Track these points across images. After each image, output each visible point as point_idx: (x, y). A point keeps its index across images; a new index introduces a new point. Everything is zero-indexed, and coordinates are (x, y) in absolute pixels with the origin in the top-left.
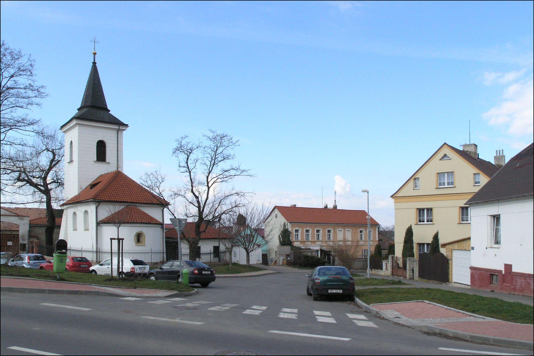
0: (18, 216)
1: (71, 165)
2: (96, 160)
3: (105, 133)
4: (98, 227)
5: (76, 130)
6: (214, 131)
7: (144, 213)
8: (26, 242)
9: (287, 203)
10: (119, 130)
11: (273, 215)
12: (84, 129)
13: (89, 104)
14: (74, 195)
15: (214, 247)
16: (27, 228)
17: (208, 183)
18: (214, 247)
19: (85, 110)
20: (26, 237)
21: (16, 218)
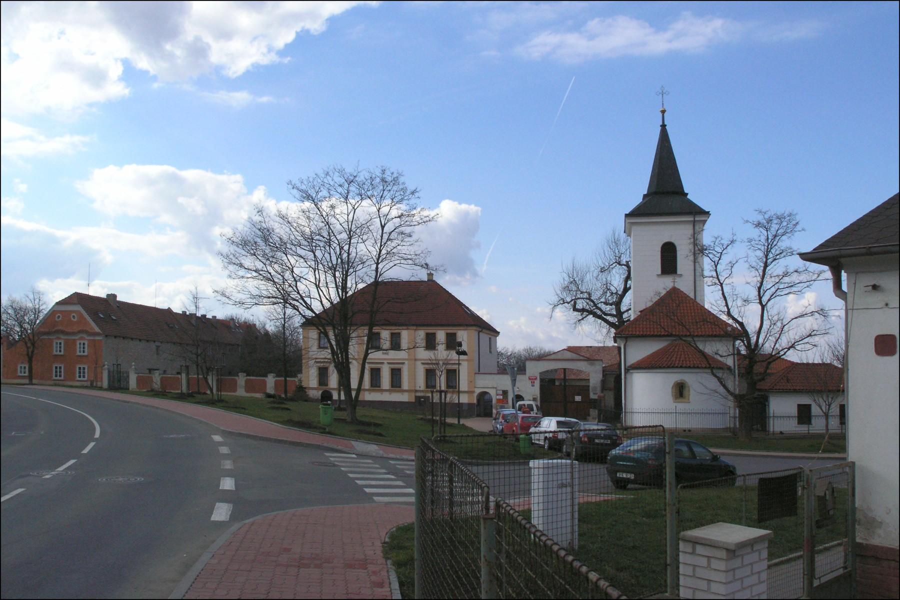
0: (588, 359)
2: (660, 273)
3: (676, 232)
6: (764, 210)
14: (162, 305)
15: (799, 405)
17: (760, 298)
18: (799, 405)
19: (647, 199)
20: (599, 389)
21: (585, 363)
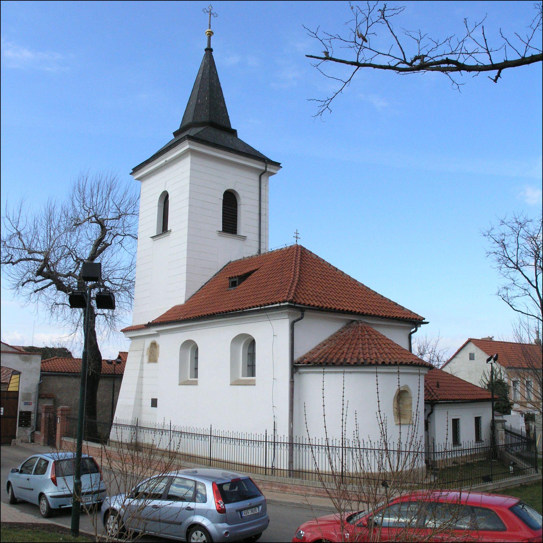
1: (164, 240)
2: (221, 230)
4: (295, 376)
5: (187, 162)
7: (384, 338)
8: (31, 408)
9: (479, 336)
10: (264, 172)
11: (465, 354)
12: (200, 161)
13: (204, 118)
16: (36, 378)
20: (34, 397)
